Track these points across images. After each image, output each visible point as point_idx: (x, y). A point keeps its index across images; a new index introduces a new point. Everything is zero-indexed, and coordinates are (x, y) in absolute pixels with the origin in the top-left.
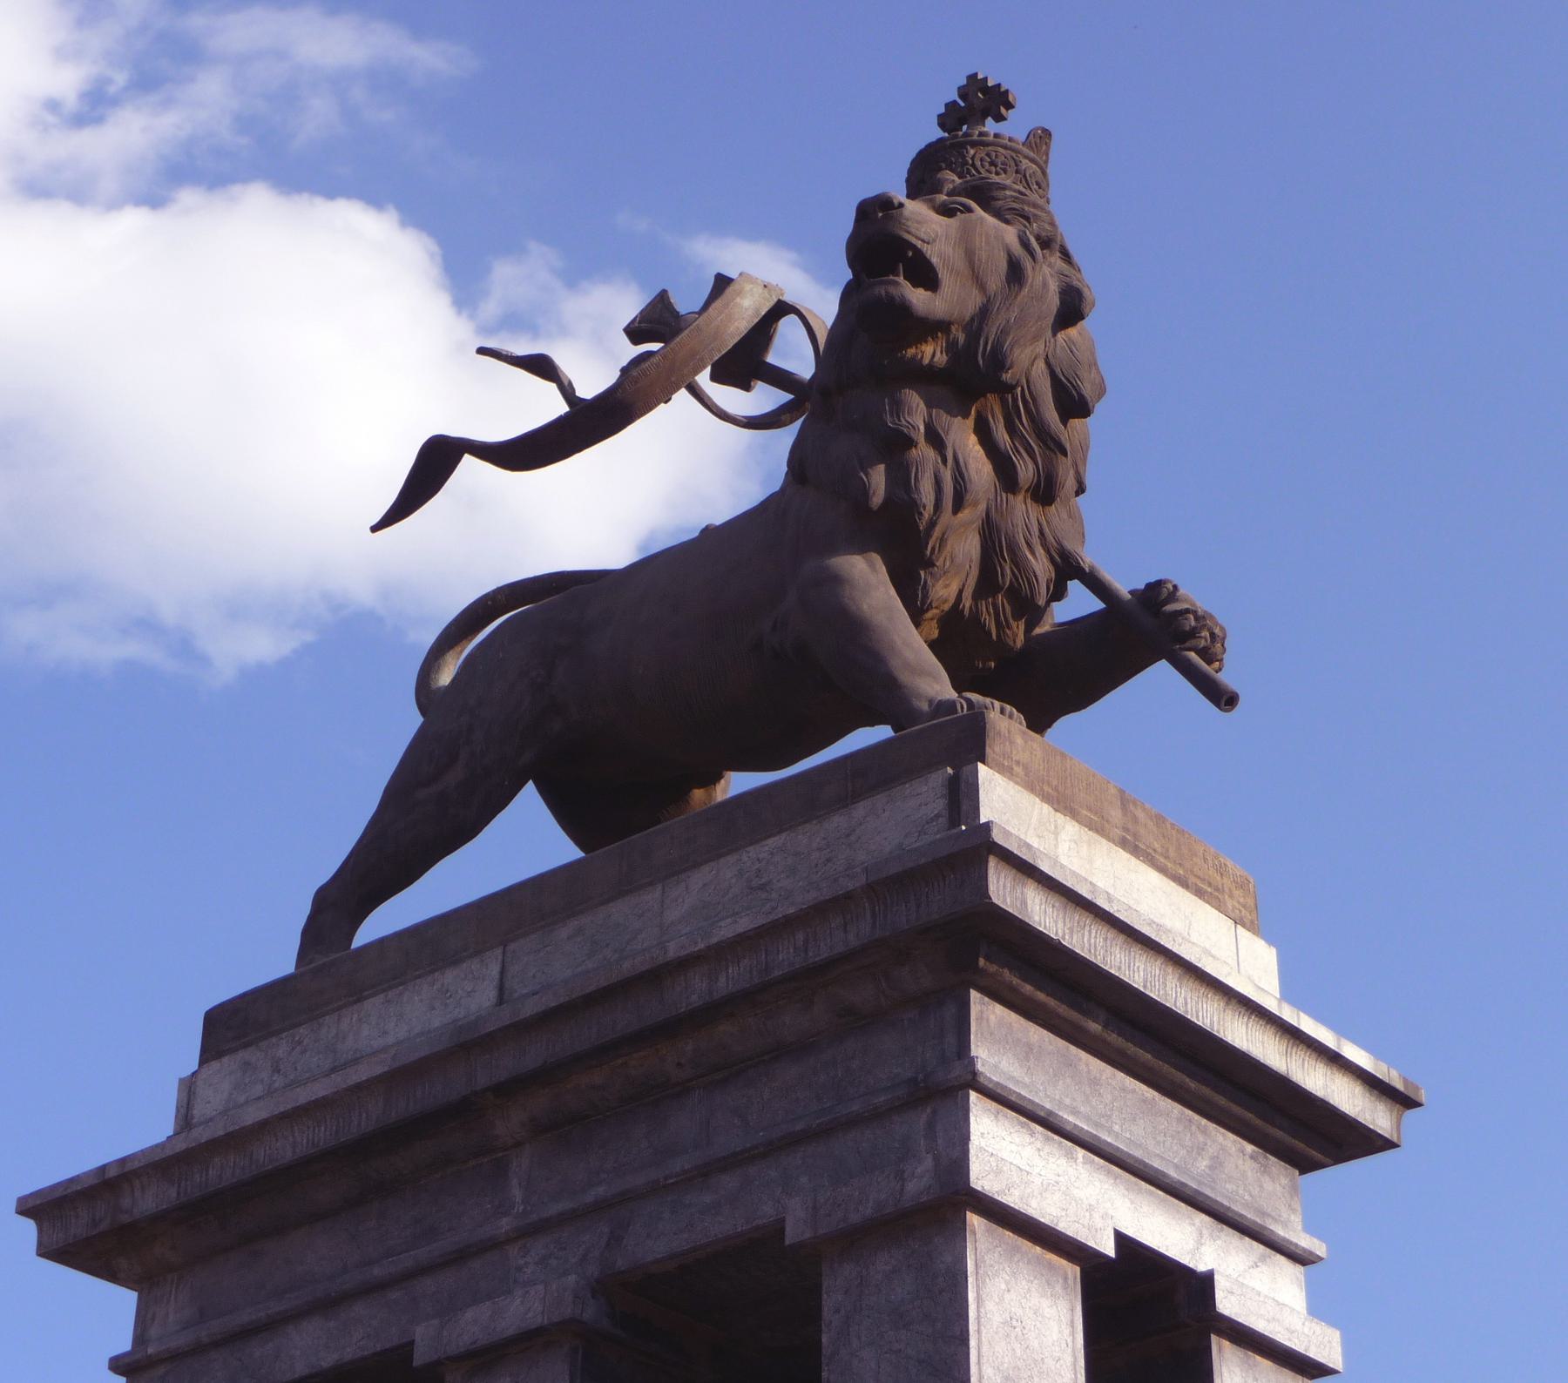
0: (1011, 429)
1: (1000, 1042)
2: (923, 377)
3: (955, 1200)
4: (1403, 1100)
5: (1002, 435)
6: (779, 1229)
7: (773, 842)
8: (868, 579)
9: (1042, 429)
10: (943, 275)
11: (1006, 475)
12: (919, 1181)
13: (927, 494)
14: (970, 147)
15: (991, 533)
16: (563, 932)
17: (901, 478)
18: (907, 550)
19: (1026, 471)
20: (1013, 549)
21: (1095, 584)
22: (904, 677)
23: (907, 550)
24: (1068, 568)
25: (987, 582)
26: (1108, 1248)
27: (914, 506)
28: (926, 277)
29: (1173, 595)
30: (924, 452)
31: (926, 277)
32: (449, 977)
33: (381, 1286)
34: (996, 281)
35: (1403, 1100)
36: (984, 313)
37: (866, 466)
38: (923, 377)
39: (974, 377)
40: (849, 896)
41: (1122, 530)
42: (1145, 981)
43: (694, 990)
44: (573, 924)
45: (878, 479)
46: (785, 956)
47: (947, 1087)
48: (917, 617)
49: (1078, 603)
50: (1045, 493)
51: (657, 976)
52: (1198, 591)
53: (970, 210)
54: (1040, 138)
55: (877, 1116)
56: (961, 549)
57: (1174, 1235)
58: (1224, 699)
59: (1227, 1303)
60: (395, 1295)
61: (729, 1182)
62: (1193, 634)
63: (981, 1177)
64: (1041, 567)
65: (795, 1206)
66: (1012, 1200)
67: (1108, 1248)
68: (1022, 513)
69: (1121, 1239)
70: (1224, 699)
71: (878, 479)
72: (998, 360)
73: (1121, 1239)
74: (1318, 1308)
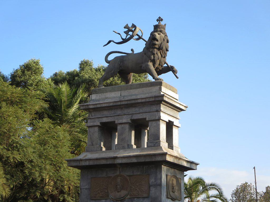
0: (162, 52)
1: (163, 108)
2: (156, 48)
3: (159, 119)
4: (186, 107)
5: (162, 53)
6: (146, 118)
7: (144, 88)
8: (151, 64)
9: (163, 50)
10: (159, 41)
11: (162, 56)
12: (157, 118)
13: (156, 59)
14: (160, 20)
15: (160, 61)
16: (126, 91)
17: (154, 57)
18: (154, 62)
19: (163, 56)
20: (162, 62)
21: (167, 64)
22: (154, 75)
23: (154, 62)
24: (165, 63)
25: (159, 65)
26: (168, 121)
27: (155, 60)
28: (157, 41)
29: (174, 68)
30: (156, 55)
31: (157, 41)
32: (116, 92)
33: (111, 116)
34: (162, 40)
35: (186, 107)
36: (161, 43)
37: (151, 55)
38: (156, 48)
39: (160, 49)
40: (153, 97)
41: (170, 60)
42: (166, 90)
43: (140, 101)
44: (127, 91)
45: (152, 57)
46: (147, 100)
47: (159, 111)
48: (154, 67)
49: (165, 65)
50: (164, 57)
51: (137, 99)
52: (176, 68)
53: (161, 34)
54: (165, 25)
55: (153, 112)
56: (158, 62)
57: (172, 119)
58: (177, 78)
59: (174, 124)
60: (113, 117)
61: (141, 114)
62: (175, 72)
63: (161, 118)
64: (163, 63)
65: (148, 117)
66: (163, 119)
67: (168, 121)
68: (163, 59)
69: (169, 120)
70: (177, 78)
71: (152, 57)
72: (162, 48)
73: (169, 120)
74: (180, 123)
